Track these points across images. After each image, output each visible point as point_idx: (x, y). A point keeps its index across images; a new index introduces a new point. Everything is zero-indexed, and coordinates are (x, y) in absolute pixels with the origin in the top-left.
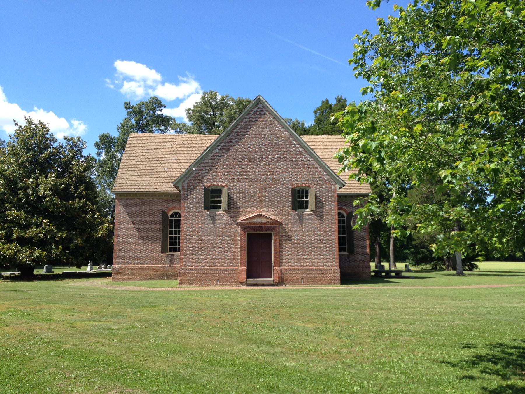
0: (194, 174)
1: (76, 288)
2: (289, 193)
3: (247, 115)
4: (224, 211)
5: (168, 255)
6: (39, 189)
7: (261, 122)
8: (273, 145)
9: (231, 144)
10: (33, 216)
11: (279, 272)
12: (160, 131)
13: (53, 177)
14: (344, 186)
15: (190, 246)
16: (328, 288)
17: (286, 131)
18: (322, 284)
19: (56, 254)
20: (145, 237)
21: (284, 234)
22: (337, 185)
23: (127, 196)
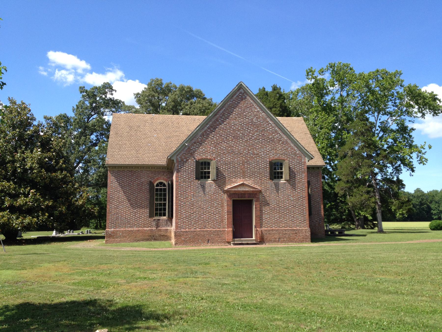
0: (186, 148)
1: (89, 250)
2: (267, 165)
3: (231, 98)
4: (212, 181)
5: (154, 220)
6: (25, 162)
7: (242, 105)
8: (253, 124)
9: (218, 123)
10: (20, 187)
11: (260, 233)
12: (111, 112)
13: (39, 151)
14: (312, 158)
15: (184, 211)
16: (304, 245)
17: (264, 112)
18: (295, 242)
19: (42, 221)
20: (134, 204)
21: (263, 200)
22: (306, 158)
23: (118, 168)
